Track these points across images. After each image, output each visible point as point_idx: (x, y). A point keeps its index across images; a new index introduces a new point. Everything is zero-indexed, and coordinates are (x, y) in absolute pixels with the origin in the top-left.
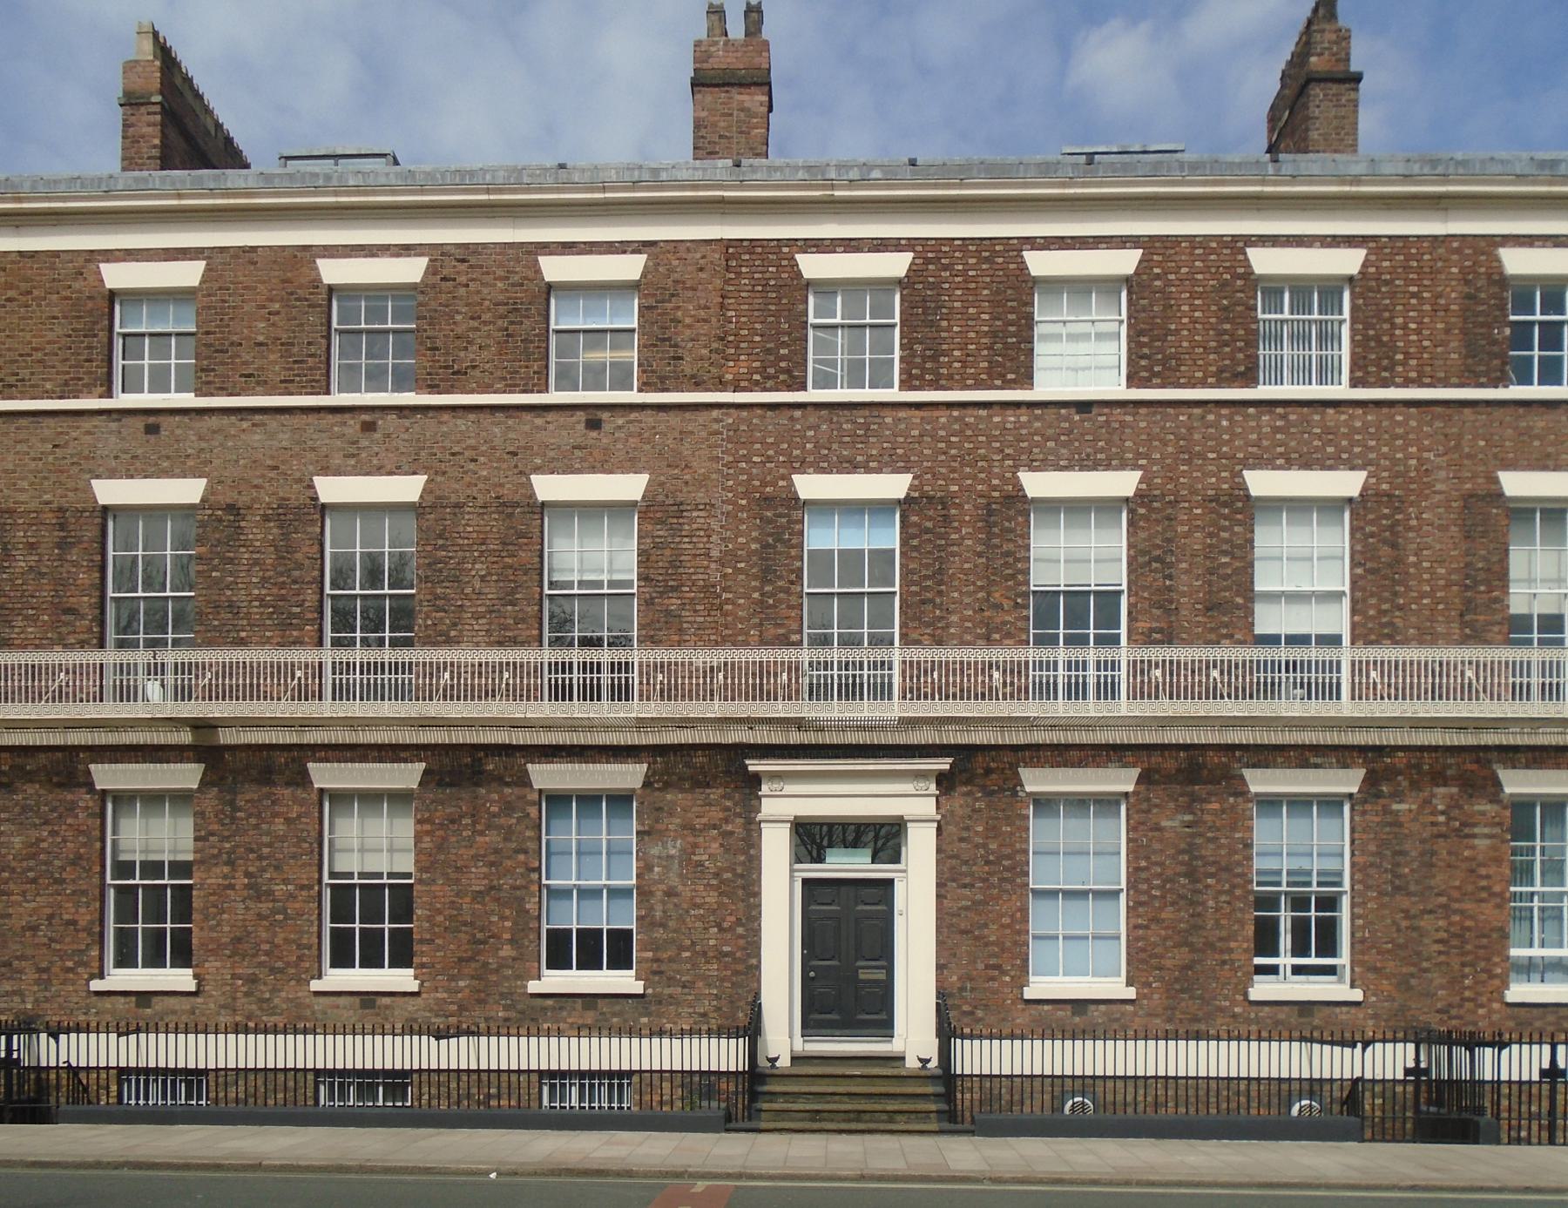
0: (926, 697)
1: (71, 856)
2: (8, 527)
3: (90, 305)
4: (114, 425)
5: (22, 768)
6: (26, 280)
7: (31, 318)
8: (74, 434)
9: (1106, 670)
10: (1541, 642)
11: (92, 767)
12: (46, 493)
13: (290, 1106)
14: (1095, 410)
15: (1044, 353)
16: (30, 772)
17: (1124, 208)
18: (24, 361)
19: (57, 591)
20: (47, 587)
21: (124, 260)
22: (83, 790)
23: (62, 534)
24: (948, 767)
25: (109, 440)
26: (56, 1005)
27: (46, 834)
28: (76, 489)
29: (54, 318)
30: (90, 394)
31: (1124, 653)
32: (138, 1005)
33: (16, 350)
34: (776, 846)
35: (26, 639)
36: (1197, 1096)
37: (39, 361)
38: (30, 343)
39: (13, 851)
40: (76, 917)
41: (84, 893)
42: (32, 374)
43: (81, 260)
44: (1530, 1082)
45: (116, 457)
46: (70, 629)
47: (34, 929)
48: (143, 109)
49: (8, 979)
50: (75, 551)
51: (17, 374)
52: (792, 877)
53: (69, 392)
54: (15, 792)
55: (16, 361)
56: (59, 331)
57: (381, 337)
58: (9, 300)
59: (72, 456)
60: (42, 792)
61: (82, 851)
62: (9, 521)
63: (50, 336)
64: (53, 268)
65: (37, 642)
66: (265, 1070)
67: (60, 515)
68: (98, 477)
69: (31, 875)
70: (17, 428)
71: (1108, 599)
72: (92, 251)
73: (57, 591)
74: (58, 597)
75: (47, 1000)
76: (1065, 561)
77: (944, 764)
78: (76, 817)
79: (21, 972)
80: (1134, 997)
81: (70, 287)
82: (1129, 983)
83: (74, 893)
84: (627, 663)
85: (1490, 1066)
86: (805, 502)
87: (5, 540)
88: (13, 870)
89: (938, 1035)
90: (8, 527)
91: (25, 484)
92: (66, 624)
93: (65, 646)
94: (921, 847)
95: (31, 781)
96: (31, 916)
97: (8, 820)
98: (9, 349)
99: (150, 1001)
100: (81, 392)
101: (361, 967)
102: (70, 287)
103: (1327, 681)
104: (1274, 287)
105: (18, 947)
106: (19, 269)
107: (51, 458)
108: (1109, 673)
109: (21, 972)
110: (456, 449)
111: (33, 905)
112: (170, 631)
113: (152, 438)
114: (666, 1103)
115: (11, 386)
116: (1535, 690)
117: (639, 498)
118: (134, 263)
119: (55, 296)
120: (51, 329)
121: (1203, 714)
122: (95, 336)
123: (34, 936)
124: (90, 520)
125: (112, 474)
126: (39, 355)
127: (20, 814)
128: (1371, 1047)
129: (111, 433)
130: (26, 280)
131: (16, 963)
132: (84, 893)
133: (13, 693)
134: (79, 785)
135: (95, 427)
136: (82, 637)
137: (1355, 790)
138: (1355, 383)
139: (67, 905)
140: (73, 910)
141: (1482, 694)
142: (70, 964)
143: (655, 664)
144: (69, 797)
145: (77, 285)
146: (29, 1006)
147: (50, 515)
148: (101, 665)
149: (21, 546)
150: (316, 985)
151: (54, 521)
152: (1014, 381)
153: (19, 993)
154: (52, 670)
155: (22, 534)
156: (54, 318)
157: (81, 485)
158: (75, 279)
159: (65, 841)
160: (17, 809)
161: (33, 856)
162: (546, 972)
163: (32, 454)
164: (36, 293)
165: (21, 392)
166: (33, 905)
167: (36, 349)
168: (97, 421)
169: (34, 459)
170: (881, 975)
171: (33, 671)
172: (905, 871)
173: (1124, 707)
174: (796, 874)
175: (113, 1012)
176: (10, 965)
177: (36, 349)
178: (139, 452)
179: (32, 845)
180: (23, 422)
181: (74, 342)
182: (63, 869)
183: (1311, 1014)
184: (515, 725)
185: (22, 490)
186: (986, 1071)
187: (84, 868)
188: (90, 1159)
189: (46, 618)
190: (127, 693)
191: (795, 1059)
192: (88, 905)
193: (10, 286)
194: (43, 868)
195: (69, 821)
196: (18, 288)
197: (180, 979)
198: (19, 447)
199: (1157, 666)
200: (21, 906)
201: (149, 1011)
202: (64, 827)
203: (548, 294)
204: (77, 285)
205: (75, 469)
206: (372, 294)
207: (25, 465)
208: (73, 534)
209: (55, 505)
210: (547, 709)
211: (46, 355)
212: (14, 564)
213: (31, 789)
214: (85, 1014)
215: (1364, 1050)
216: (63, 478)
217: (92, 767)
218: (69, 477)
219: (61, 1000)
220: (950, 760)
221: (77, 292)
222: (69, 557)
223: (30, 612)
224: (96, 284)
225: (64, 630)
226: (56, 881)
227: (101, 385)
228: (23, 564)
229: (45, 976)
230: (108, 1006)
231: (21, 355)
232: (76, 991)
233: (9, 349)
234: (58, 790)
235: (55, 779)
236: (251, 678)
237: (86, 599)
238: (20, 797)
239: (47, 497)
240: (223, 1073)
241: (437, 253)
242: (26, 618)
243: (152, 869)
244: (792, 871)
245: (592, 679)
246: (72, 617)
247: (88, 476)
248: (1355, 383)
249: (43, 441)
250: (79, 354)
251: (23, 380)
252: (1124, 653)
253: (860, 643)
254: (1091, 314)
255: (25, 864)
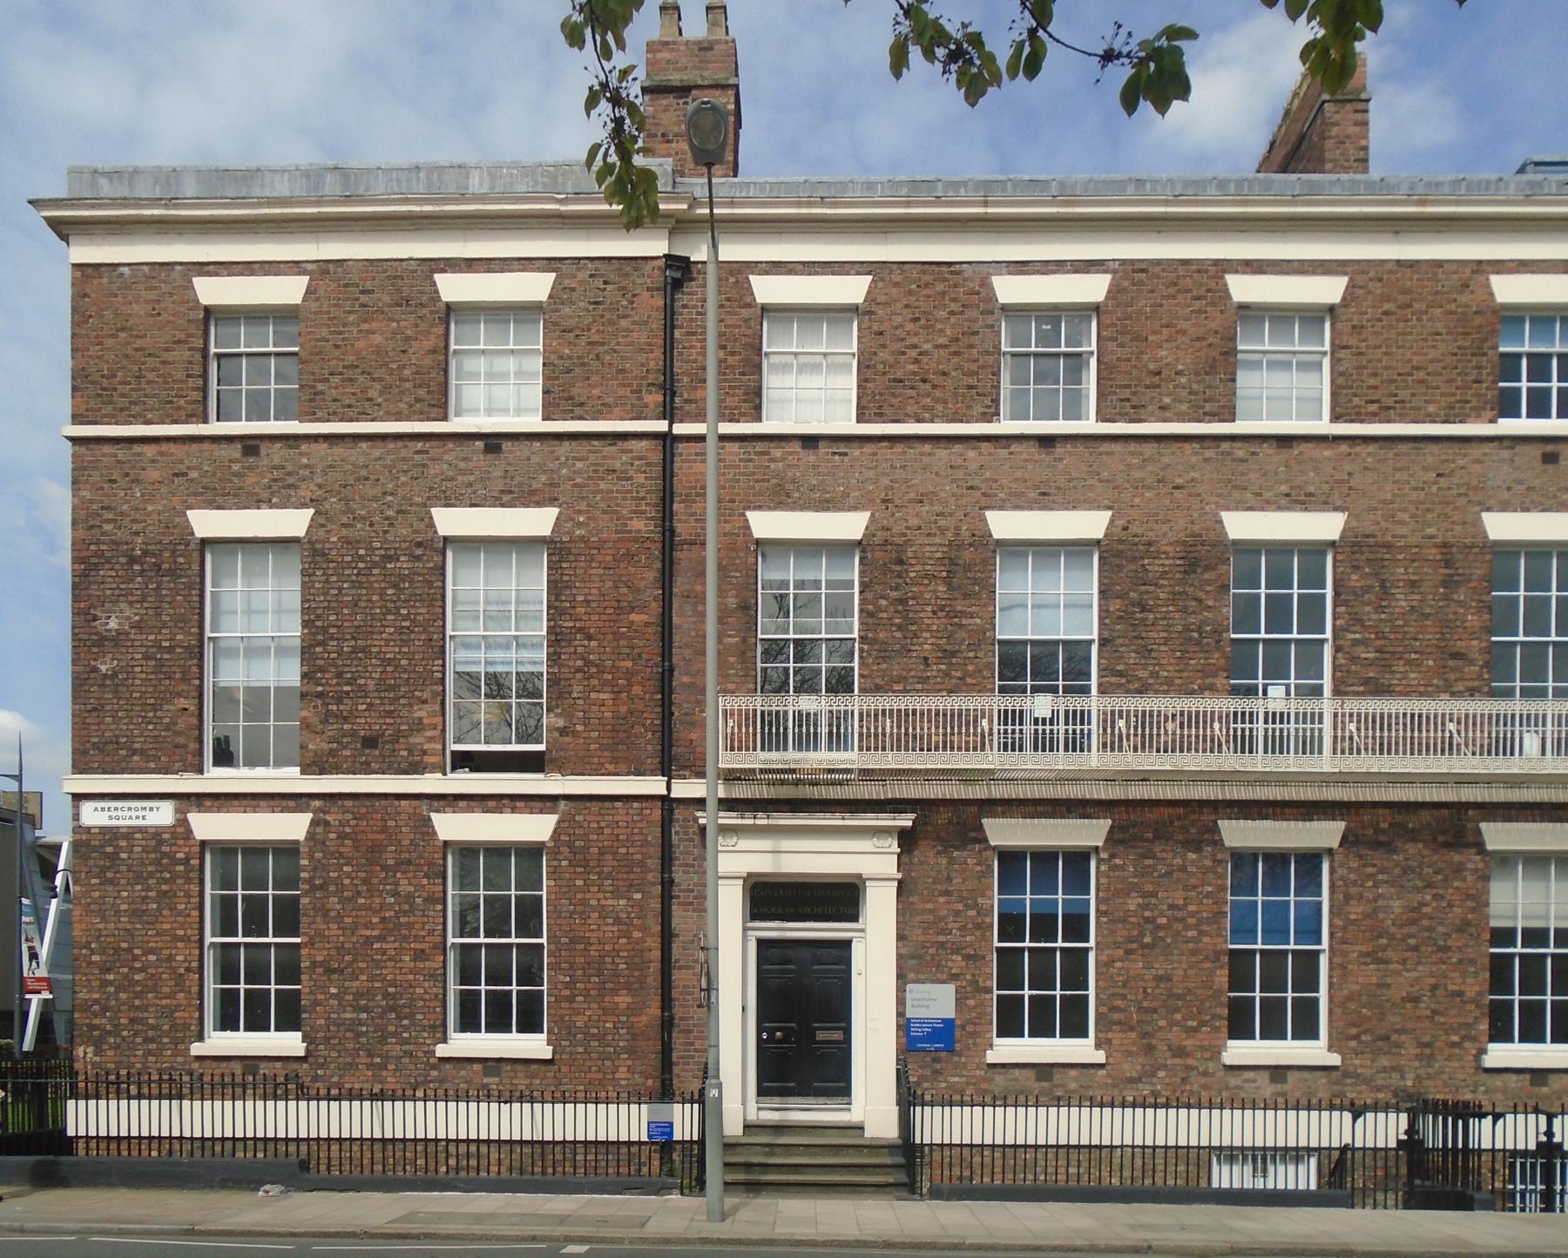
0: (975, 749)
1: (1458, 922)
2: (1386, 563)
3: (1478, 320)
4: (1506, 454)
5: (1403, 826)
6: (1405, 292)
7: (1411, 333)
8: (1461, 462)
9: (1304, 723)
10: (1002, 690)
11: (1483, 826)
12: (1429, 526)
13: (483, 1174)
14: (821, 444)
15: (774, 384)
16: (1412, 831)
17: (219, 232)
18: (1404, 381)
19: (1442, 634)
20: (1433, 630)
21: (1518, 272)
22: (1473, 851)
23: (1447, 571)
24: (910, 823)
25: (1500, 472)
26: (1440, 1083)
27: (1428, 898)
28: (1464, 523)
29: (1438, 334)
30: (1478, 418)
31: (1094, 703)
32: (1532, 1084)
33: (1395, 368)
34: (730, 903)
35: (1409, 685)
36: (329, 1158)
37: (1422, 382)
38: (1410, 361)
39: (1392, 916)
40: (1463, 988)
41: (1471, 962)
42: (1413, 395)
43: (1468, 270)
44: (1386, 1149)
45: (1509, 489)
46: (1458, 675)
47: (1415, 1000)
48: (1348, 107)
49: (1388, 1053)
50: (1462, 590)
51: (1396, 395)
52: (745, 937)
53: (1456, 415)
54: (1395, 851)
55: (1396, 381)
56: (1442, 348)
57: (236, 359)
58: (1386, 313)
59: (1459, 486)
60: (1426, 852)
61: (1469, 916)
62: (1387, 556)
63: (1433, 354)
64: (1435, 279)
65: (1422, 689)
66: (564, 1142)
67: (1446, 551)
68: (1488, 509)
69: (1412, 941)
70: (1396, 455)
71: (1077, 650)
72: (1480, 262)
73: (1442, 634)
74: (1444, 640)
75: (1429, 1076)
76: (1033, 607)
77: (906, 821)
78: (1464, 880)
79: (1399, 1046)
80: (1103, 1061)
81: (1455, 300)
82: (1098, 1046)
83: (1460, 962)
84: (1082, 712)
85: (1485, 1134)
86: (999, 543)
87: (1384, 577)
88: (1392, 937)
89: (899, 1103)
90: (1386, 563)
91: (1405, 517)
92: (1454, 670)
93: (1453, 694)
94: (880, 906)
95: (1414, 840)
96: (1412, 986)
97: (1387, 882)
98: (1387, 368)
99: (1285, 1075)
100: (1468, 416)
101: (1293, 1038)
102: (1455, 300)
103: (1502, 736)
104: (1251, 313)
105: (1397, 1019)
106: (1398, 280)
107: (1434, 489)
108: (1278, 726)
109: (1399, 1046)
110: (1179, 481)
111: (1415, 974)
112: (1551, 678)
113: (1550, 468)
114: (463, 1169)
115: (1390, 408)
116: (1028, 743)
117: (1100, 536)
118: (1529, 275)
119: (1439, 310)
120: (1434, 347)
121: (1375, 770)
122: (1484, 354)
123: (1416, 1007)
124: (1480, 557)
125: (1505, 507)
126: (1421, 375)
127: (1400, 876)
128: (1361, 1119)
129: (1503, 460)
130: (1405, 292)
131: (1394, 1037)
132: (1471, 962)
133: (1397, 744)
134: (1467, 846)
135: (1485, 454)
136: (1471, 684)
137: (1100, 844)
138: (1336, 418)
139: (1453, 975)
140: (1460, 980)
141: (1224, 747)
142: (1455, 1038)
143: (884, 711)
144: (1457, 858)
145: (1463, 298)
146: (1409, 1083)
147: (1434, 551)
148: (1021, 712)
149: (1401, 584)
150: (197, 1049)
151: (1439, 557)
152: (1375, 415)
153: (1399, 1069)
154: (1442, 720)
155: (1402, 570)
156: (1438, 334)
157: (1469, 518)
158: (1461, 292)
159: (1450, 905)
160: (1397, 871)
161: (1413, 922)
162: (997, 1041)
163: (1413, 483)
164: (1416, 306)
165: (1400, 415)
166: (1415, 974)
167: (1418, 368)
168: (1487, 448)
169: (1416, 489)
170: (837, 1036)
171: (1417, 720)
172: (863, 930)
173: (1094, 759)
174: (750, 933)
175: (1504, 1091)
176: (1388, 1038)
177: (1418, 368)
178: (1536, 483)
179: (1413, 910)
180: (1403, 448)
181: (1460, 361)
182: (1448, 935)
183: (1284, 1080)
184: (1144, 777)
185: (1402, 523)
186: (591, 1138)
187: (1471, 935)
188: (1313, 1247)
189: (1431, 663)
190: (1505, 747)
191: (748, 1127)
192: (1476, 973)
193: (1388, 299)
194: (1426, 934)
195: (1456, 884)
196: (1396, 301)
197: (290, 1043)
198: (1398, 476)
199: (983, 717)
200: (1401, 975)
201: (1545, 1090)
202: (1450, 891)
203: (448, 315)
204: (1463, 298)
205: (1462, 502)
206: (1276, 314)
207: (1405, 495)
208: (1461, 571)
209: (1439, 540)
210: (1230, 761)
211: (1428, 374)
212: (1393, 603)
213: (1412, 848)
214: (1473, 1092)
215: (1354, 1121)
216: (1448, 510)
217: (1483, 826)
218: (1456, 509)
219: (1445, 1077)
220: (913, 816)
221: (1461, 306)
222: (1455, 597)
223: (1413, 656)
224: (1486, 297)
225: (1452, 676)
226: (1441, 949)
227: (1492, 409)
228: (1403, 603)
229: (1428, 1051)
230: (1499, 1083)
231: (1400, 374)
232: (1462, 1068)
233: (1387, 368)
234: (1444, 851)
235: (1441, 838)
236: (1151, 729)
237: (1475, 643)
238: (1401, 857)
239: (1430, 531)
240: (637, 1147)
241: (322, 270)
242: (1409, 662)
243: (1535, 936)
244: (745, 929)
245: (1274, 730)
246: (1461, 663)
247: (1477, 509)
248: (1336, 418)
249: (1425, 469)
250: (1466, 374)
251: (1403, 401)
252: (1327, 705)
253: (1546, 695)
254: (1553, 346)
255: (1405, 930)
